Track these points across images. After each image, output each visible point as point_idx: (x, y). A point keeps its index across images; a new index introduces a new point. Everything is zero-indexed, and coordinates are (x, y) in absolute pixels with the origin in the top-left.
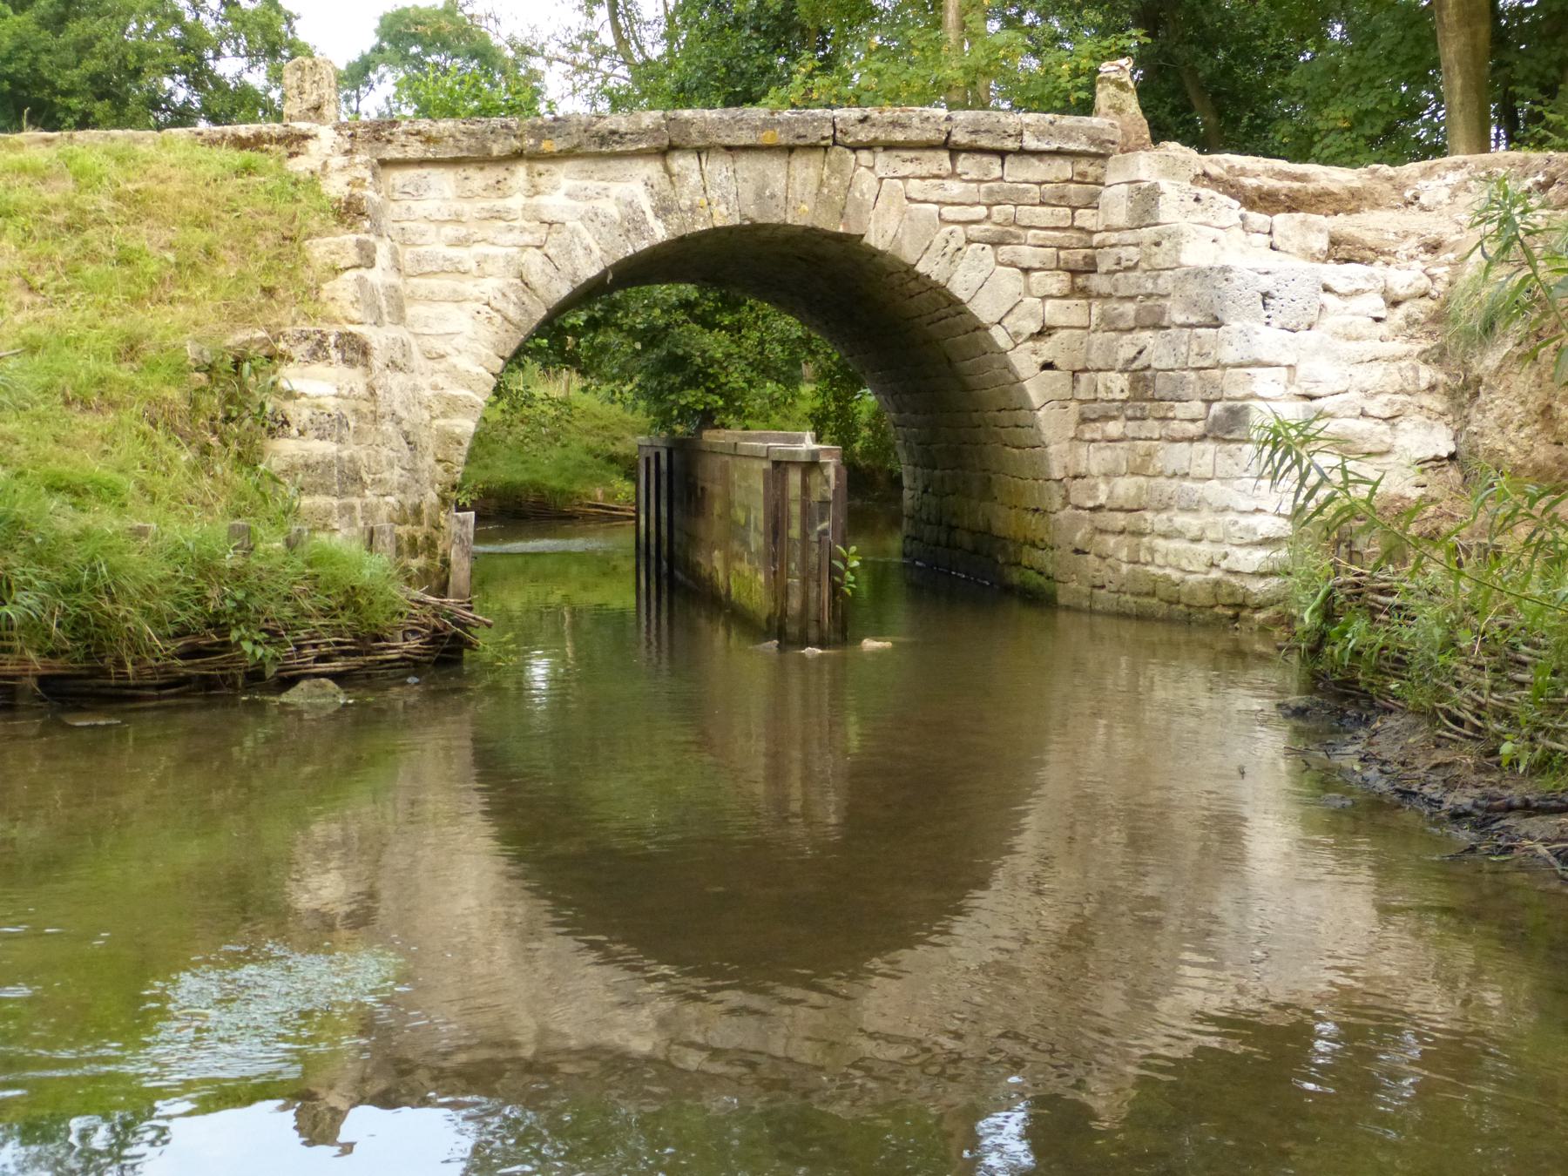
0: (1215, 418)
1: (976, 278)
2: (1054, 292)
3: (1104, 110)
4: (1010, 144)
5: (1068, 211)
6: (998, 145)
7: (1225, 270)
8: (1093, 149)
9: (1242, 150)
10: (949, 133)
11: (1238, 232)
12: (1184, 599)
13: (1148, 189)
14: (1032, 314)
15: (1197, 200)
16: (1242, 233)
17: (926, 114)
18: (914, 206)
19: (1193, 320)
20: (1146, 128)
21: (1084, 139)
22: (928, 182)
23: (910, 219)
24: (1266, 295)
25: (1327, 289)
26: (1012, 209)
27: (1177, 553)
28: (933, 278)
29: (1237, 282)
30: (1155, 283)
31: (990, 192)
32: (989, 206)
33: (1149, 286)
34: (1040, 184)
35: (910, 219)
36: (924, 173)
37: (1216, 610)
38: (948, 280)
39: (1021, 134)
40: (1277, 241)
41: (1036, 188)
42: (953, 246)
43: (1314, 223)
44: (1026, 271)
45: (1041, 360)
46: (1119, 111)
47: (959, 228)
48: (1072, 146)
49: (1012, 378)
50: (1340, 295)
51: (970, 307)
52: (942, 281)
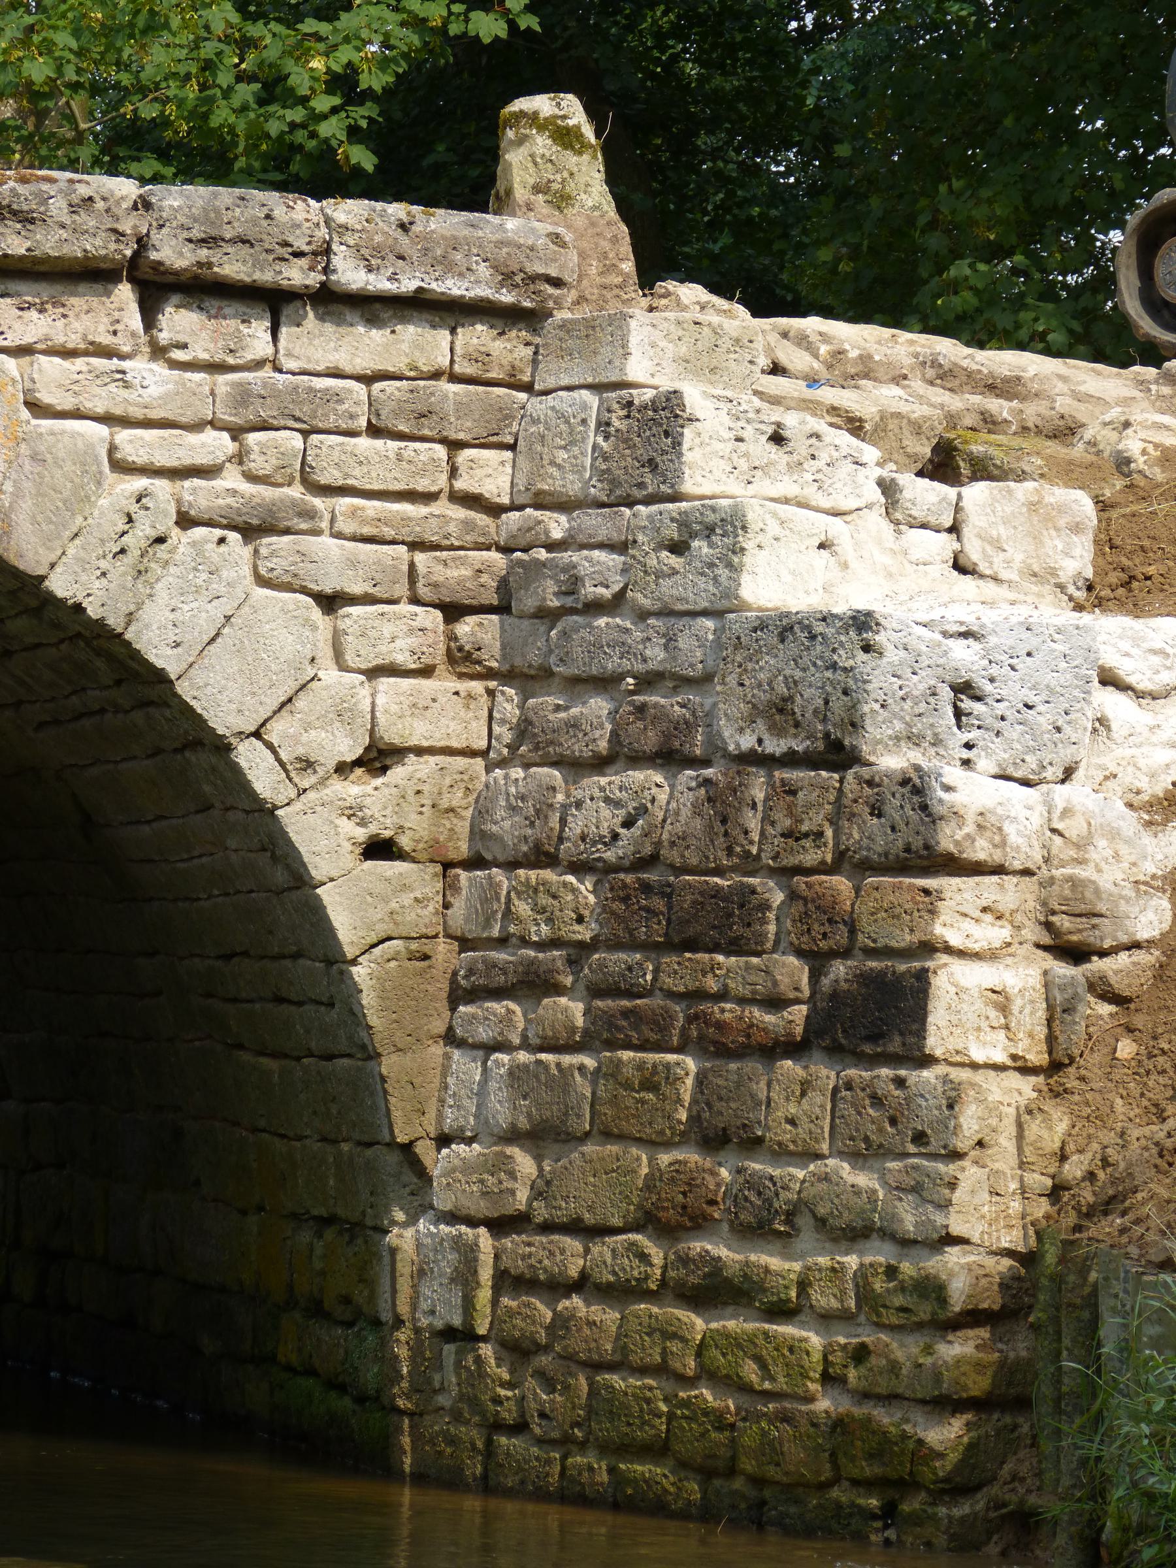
0: (834, 995)
1: (205, 616)
2: (403, 659)
3: (521, 194)
4: (297, 275)
5: (440, 451)
6: (265, 277)
7: (862, 622)
8: (507, 297)
9: (858, 313)
10: (142, 243)
11: (876, 521)
12: (748, 1465)
13: (654, 406)
14: (343, 714)
15: (777, 439)
16: (887, 527)
17: (83, 191)
18: (46, 424)
19: (775, 746)
20: (626, 247)
21: (483, 270)
22: (80, 363)
23: (35, 457)
24: (964, 689)
25: (1109, 679)
26: (297, 441)
27: (735, 1343)
28: (93, 612)
29: (893, 655)
30: (670, 641)
31: (243, 396)
32: (236, 433)
33: (656, 655)
34: (368, 379)
35: (35, 457)
36: (74, 341)
37: (835, 1493)
38: (130, 617)
39: (327, 251)
40: (974, 552)
41: (359, 389)
42: (144, 530)
43: (1061, 509)
44: (330, 602)
45: (361, 834)
46: (561, 200)
47: (161, 487)
48: (454, 287)
49: (280, 877)
50: (1139, 695)
51: (183, 689)
52: (115, 622)
